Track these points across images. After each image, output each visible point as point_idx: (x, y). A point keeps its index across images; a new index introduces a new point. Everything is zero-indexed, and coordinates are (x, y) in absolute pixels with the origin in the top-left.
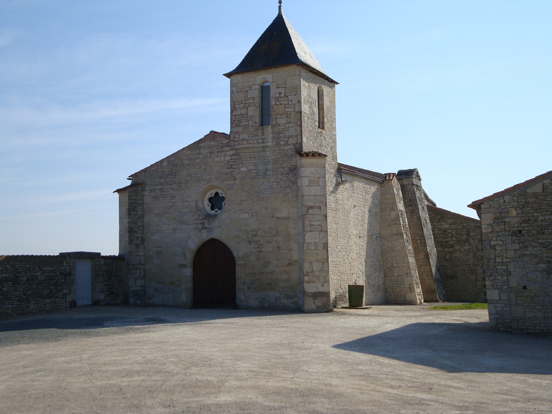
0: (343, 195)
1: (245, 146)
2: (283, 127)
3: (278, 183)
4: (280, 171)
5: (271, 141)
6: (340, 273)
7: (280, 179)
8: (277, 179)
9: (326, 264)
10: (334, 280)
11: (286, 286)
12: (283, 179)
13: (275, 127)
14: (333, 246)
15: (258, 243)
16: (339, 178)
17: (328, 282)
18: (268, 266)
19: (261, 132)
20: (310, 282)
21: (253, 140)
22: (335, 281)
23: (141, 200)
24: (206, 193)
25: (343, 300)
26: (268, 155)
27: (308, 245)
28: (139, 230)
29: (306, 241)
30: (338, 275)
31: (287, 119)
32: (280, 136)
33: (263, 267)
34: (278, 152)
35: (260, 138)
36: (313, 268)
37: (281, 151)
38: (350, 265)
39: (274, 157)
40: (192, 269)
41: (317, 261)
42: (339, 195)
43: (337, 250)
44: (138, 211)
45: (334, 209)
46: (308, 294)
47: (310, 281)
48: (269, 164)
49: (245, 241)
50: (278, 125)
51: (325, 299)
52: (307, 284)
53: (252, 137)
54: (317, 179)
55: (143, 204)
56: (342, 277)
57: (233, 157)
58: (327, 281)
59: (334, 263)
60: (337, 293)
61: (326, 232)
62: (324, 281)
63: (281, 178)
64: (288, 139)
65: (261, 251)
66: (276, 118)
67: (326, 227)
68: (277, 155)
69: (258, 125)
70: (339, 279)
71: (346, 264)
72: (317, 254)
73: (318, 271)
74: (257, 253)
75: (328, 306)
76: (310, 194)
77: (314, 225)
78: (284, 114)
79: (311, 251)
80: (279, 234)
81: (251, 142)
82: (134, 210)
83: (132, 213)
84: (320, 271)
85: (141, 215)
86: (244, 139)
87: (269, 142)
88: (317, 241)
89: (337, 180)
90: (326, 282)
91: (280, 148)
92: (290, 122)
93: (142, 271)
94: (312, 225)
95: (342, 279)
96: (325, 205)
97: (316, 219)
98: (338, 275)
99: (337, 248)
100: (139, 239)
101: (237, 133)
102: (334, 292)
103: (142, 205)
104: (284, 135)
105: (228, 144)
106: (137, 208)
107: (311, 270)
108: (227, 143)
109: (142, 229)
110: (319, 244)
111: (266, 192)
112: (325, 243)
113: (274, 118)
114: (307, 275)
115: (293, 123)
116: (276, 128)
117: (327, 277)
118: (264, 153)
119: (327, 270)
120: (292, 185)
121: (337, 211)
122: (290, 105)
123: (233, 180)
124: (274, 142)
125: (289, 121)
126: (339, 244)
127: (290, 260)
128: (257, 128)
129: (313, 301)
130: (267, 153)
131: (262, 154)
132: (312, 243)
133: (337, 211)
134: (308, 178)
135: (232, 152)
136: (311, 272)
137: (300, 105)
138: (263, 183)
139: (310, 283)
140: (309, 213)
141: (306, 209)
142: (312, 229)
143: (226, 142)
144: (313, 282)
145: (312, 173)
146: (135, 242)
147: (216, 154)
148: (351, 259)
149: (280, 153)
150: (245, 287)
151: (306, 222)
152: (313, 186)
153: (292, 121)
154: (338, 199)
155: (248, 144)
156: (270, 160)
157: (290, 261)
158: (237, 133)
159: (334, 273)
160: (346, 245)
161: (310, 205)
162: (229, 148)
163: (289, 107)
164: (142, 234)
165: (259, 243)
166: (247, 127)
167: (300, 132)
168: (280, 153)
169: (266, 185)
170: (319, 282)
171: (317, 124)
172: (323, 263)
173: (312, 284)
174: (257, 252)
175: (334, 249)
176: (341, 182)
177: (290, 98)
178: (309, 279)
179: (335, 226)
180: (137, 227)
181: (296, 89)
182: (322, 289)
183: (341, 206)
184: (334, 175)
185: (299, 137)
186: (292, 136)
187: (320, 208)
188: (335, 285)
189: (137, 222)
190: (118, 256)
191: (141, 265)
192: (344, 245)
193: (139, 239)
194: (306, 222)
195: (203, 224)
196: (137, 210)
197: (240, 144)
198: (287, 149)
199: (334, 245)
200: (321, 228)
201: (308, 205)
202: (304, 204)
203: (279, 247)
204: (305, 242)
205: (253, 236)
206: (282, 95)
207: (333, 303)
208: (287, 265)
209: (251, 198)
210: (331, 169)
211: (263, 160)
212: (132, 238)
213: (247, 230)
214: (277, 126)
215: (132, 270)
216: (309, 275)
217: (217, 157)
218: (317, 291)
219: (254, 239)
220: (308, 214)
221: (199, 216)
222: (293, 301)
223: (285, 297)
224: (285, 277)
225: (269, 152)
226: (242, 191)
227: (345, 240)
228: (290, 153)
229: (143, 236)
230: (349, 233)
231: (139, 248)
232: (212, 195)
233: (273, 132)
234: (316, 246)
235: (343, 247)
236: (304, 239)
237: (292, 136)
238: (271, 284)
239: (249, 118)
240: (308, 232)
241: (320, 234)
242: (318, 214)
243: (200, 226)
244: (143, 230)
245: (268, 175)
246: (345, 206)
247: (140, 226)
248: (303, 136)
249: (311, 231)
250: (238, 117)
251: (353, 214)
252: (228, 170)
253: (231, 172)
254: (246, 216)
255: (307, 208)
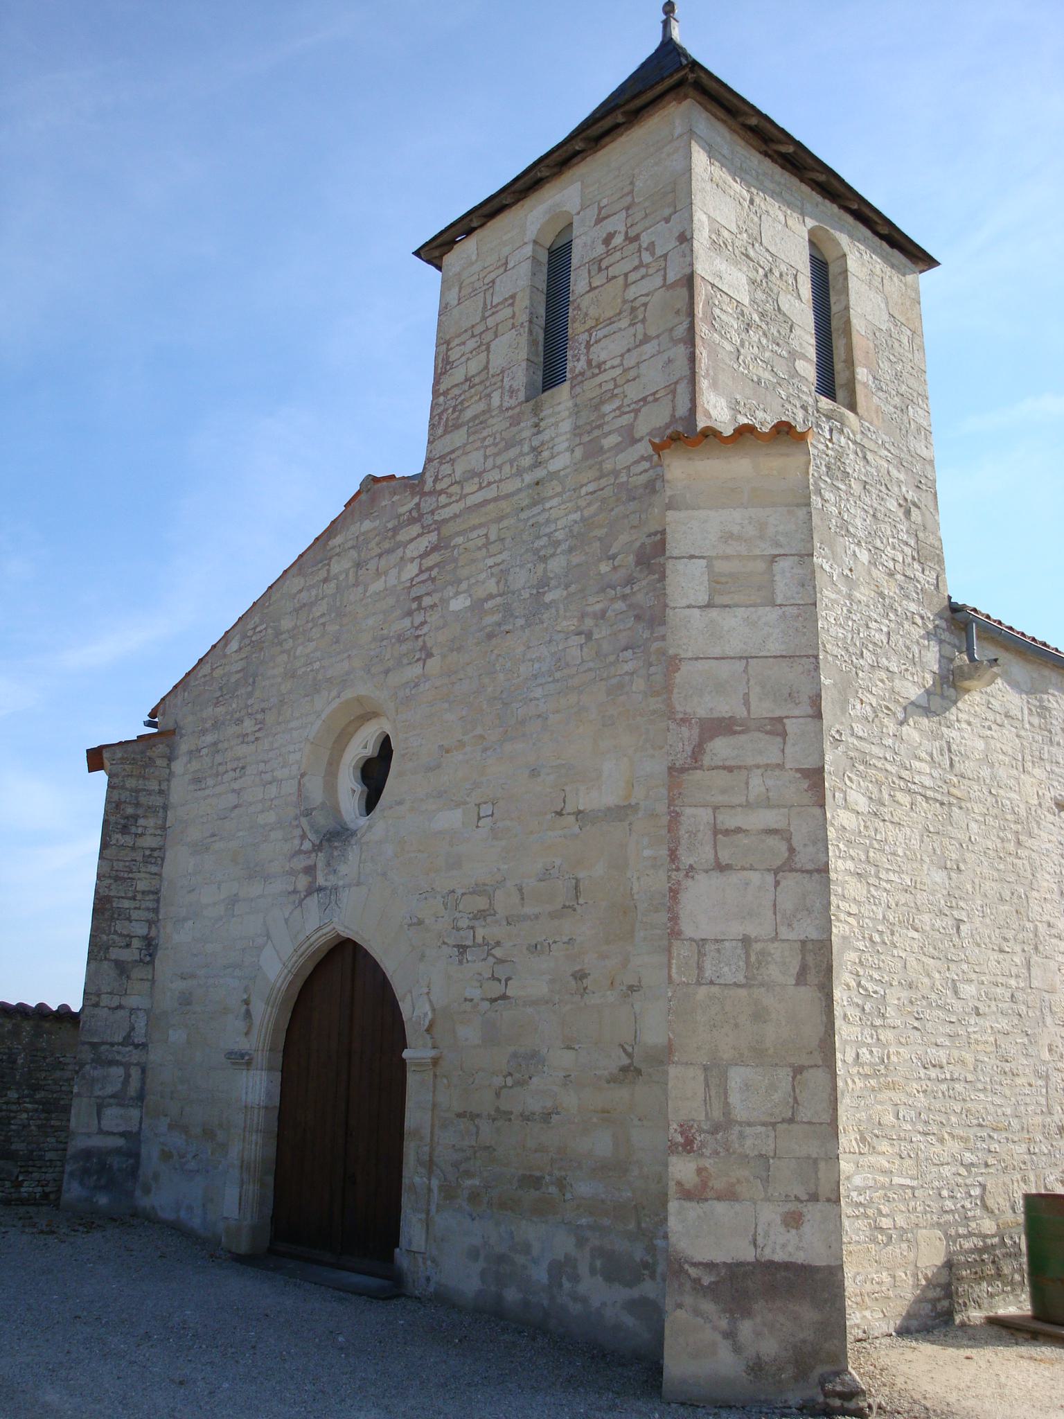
0: (992, 742)
1: (471, 501)
2: (619, 371)
3: (589, 636)
4: (599, 574)
5: (567, 450)
6: (980, 1125)
7: (595, 616)
8: (583, 616)
9: (816, 1077)
10: (934, 1169)
11: (603, 1201)
12: (609, 613)
13: (582, 382)
14: (926, 980)
15: (494, 956)
16: (961, 653)
17: (829, 1200)
18: (530, 1078)
19: (529, 423)
20: (711, 1194)
21: (500, 467)
22: (947, 1171)
23: (161, 792)
24: (342, 740)
25: (999, 1275)
26: (554, 513)
27: (701, 954)
28: (139, 909)
29: (688, 930)
30: (965, 1140)
31: (632, 330)
32: (604, 415)
33: (509, 1081)
34: (591, 488)
35: (526, 449)
36: (731, 1100)
37: (603, 482)
38: (1040, 1082)
39: (576, 516)
40: (278, 1076)
41: (758, 1055)
42: (966, 736)
43: (958, 1005)
44: (142, 835)
45: (930, 793)
46: (693, 1272)
47: (704, 1185)
48: (553, 555)
49: (444, 943)
50: (597, 371)
51: (809, 1314)
52: (687, 1204)
53: (496, 455)
54: (761, 566)
55: (165, 808)
56: (995, 1146)
57: (429, 562)
58: (824, 1190)
59: (933, 1073)
60: (959, 1236)
61: (816, 876)
62: (800, 1191)
63: (598, 607)
64: (635, 418)
65: (504, 997)
66: (588, 342)
67: (814, 843)
68: (589, 505)
69: (522, 396)
70: (969, 1157)
71: (1019, 1081)
72: (760, 1015)
73: (764, 1124)
74: (487, 1004)
75: (827, 1368)
76: (717, 651)
77: (738, 830)
78: (619, 314)
79: (714, 989)
80: (581, 901)
81: (494, 475)
82: (125, 830)
83: (113, 842)
84: (774, 1125)
85: (153, 850)
86: (473, 474)
87: (559, 454)
88: (758, 929)
89: (945, 659)
90: (814, 1198)
91: (601, 470)
92: (646, 339)
93: (135, 1073)
94: (727, 832)
95: (991, 1161)
96: (810, 711)
97: (751, 798)
98: (965, 1140)
99: (956, 992)
100: (136, 943)
101: (448, 459)
102: (939, 1233)
103: (160, 814)
104: (617, 403)
105: (415, 514)
106: (141, 822)
107: (717, 1114)
108: (410, 512)
109: (151, 905)
110: (772, 947)
111: (538, 693)
112: (810, 946)
113: (583, 346)
114: (688, 1146)
115: (658, 336)
116: (588, 385)
117: (822, 1165)
118: (540, 507)
119: (826, 1118)
120: (646, 634)
121: (955, 809)
122: (647, 266)
123: (418, 660)
124: (577, 449)
125: (640, 337)
126: (974, 976)
127: (630, 1049)
128: (517, 410)
129: (724, 1324)
130: (548, 506)
131: (529, 518)
132: (727, 944)
133: (955, 809)
134: (703, 562)
135: (424, 543)
136: (714, 1130)
137: (687, 252)
138: (529, 648)
139: (706, 1200)
140: (707, 761)
141: (689, 735)
142: (725, 857)
143: (412, 505)
144: (729, 1195)
145: (728, 537)
146: (115, 953)
147: (372, 566)
148: (1046, 1056)
149: (602, 489)
150: (435, 1183)
151: (688, 811)
152: (737, 606)
153: (652, 332)
154: (954, 747)
155: (481, 488)
156: (557, 534)
157: (630, 1056)
158: (448, 459)
159: (934, 1128)
160: (1013, 982)
161: (715, 715)
162: (415, 529)
163: (643, 277)
164: (151, 923)
165: (498, 952)
166: (481, 423)
167: (687, 368)
168: (602, 489)
169: (539, 659)
170: (768, 1199)
171: (808, 370)
172: (798, 1070)
173: (720, 1208)
174: (487, 1000)
175: (933, 996)
176: (966, 669)
177: (645, 240)
178: (700, 1171)
179: (938, 880)
180: (130, 894)
181: (674, 191)
182: (784, 1246)
183: (976, 787)
184: (928, 633)
185: (682, 389)
186: (650, 398)
187: (776, 728)
188: (945, 1193)
189: (130, 875)
190: (57, 1011)
191: (130, 1048)
192: (1000, 979)
193: (136, 943)
194: (688, 811)
195: (310, 870)
196: (140, 831)
197: (454, 498)
198: (628, 464)
199: (937, 976)
200: (783, 847)
201: (702, 713)
202: (678, 708)
203: (580, 976)
204: (679, 933)
205: (475, 918)
206: (618, 240)
207: (927, 1301)
208: (612, 1080)
209: (479, 731)
210: (907, 597)
211: (533, 543)
212: (104, 937)
213: (453, 891)
214: (594, 376)
215: (88, 1067)
216: (703, 1145)
217: (378, 574)
218: (749, 1255)
219: (480, 932)
220: (701, 768)
221: (303, 837)
222: (635, 1293)
223: (598, 1263)
224: (601, 1144)
225: (555, 502)
226: (446, 705)
227: (1006, 956)
228: (643, 479)
229: (153, 934)
230: (1029, 925)
231: (128, 977)
232: (365, 747)
233: (576, 405)
234: (753, 959)
235: (999, 990)
236: (674, 919)
237: (654, 394)
238: (534, 1182)
239: (491, 385)
240: (701, 877)
241: (777, 883)
242: (767, 766)
243: (302, 882)
244: (156, 911)
245: (547, 606)
246: (1001, 792)
247: (143, 892)
248: (704, 384)
249: (721, 868)
250: (456, 391)
251: (1051, 838)
252: (407, 622)
253: (417, 628)
254: (451, 819)
255: (696, 731)
